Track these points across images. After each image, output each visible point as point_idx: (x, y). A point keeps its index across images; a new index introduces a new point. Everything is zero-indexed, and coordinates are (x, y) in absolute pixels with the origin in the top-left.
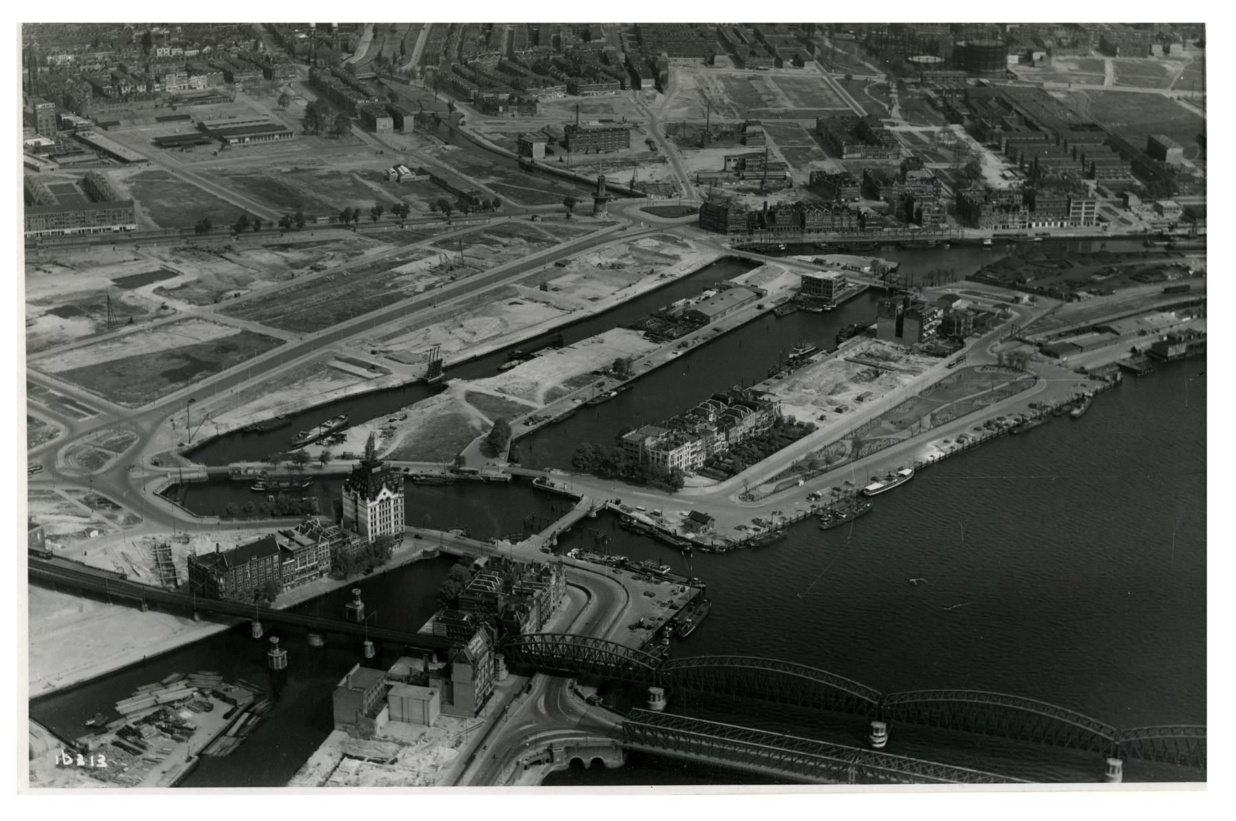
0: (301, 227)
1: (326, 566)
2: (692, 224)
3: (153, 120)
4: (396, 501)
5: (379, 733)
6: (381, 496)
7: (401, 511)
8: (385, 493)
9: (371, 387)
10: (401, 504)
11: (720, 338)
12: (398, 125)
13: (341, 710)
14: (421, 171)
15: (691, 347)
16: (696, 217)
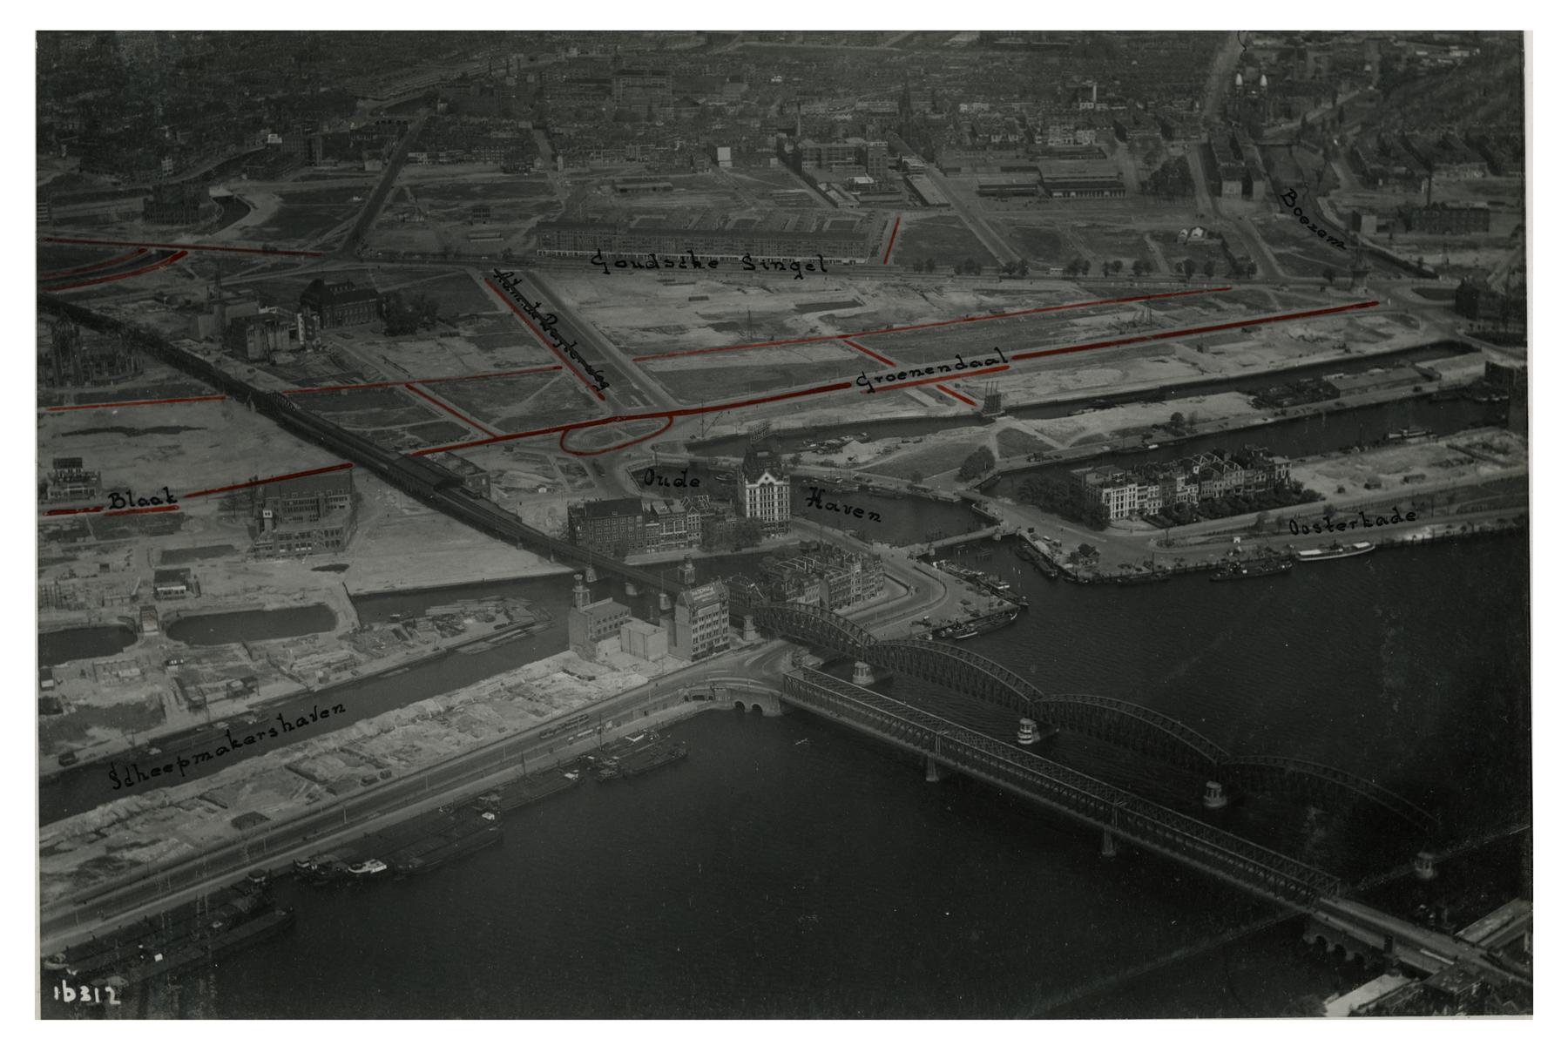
0: (1023, 274)
1: (696, 537)
2: (1447, 308)
3: (997, 169)
4: (780, 488)
5: (601, 657)
6: (762, 480)
7: (786, 497)
8: (767, 478)
9: (922, 414)
10: (786, 491)
11: (1340, 413)
12: (1247, 191)
13: (576, 632)
14: (1211, 235)
15: (1289, 416)
16: (1451, 302)
